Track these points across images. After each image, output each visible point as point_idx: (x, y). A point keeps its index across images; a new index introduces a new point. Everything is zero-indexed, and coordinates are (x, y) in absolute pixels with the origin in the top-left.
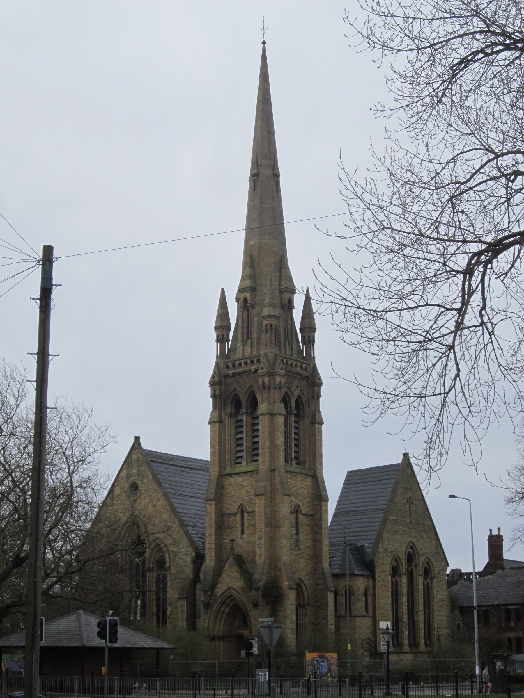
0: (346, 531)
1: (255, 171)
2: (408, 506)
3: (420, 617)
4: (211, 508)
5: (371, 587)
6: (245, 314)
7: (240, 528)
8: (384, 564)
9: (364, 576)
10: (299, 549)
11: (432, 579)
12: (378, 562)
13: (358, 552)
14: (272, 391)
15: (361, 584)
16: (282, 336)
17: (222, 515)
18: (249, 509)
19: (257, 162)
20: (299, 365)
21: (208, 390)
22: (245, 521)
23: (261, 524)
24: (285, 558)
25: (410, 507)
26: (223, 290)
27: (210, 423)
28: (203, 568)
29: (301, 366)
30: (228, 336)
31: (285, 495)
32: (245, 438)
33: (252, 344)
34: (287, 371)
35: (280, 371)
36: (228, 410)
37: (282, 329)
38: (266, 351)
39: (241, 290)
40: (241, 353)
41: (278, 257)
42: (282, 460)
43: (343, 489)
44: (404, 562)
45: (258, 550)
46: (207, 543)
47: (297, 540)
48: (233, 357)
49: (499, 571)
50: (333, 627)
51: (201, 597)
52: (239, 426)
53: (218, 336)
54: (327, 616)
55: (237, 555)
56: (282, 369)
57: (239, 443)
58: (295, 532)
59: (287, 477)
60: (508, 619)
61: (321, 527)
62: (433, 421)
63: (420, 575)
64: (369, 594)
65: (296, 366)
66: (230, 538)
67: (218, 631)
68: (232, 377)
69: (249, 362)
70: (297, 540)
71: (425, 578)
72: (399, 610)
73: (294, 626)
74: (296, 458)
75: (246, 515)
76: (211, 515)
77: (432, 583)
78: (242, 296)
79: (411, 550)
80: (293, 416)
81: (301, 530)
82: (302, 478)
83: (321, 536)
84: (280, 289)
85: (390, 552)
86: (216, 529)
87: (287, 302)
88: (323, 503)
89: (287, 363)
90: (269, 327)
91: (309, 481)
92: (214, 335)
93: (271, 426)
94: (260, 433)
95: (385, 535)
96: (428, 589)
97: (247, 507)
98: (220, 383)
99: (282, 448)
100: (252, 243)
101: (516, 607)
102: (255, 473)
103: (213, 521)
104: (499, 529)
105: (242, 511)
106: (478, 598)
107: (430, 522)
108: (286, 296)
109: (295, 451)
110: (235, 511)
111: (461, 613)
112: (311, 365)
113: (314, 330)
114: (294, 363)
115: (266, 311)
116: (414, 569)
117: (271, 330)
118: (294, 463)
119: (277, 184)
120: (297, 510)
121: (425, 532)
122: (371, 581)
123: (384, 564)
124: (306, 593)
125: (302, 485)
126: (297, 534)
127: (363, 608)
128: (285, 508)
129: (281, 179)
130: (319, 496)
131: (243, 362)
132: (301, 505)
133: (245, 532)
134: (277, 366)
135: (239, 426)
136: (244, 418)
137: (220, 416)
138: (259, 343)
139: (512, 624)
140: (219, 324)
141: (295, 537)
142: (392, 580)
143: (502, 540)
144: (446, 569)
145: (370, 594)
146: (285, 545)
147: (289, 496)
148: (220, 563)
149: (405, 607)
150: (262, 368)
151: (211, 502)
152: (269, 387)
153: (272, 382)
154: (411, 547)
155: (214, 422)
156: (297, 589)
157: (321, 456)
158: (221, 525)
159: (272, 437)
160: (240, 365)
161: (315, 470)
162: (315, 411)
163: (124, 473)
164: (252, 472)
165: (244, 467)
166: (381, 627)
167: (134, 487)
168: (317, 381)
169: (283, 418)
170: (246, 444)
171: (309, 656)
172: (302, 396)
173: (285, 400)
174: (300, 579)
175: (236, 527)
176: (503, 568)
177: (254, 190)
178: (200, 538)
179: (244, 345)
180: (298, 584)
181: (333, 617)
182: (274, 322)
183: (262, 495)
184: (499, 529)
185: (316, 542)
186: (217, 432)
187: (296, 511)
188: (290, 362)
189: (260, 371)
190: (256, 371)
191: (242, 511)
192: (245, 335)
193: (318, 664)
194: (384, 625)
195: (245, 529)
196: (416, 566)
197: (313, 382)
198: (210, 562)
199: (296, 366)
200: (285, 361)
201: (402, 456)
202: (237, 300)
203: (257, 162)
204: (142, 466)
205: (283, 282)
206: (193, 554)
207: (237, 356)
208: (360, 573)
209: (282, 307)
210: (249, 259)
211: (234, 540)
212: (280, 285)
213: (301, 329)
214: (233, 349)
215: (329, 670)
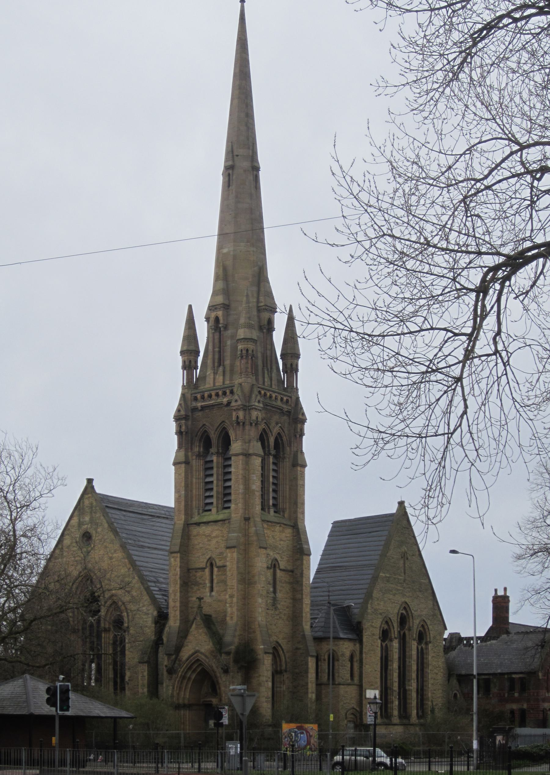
1: (230, 163)
2: (402, 562)
3: (413, 686)
4: (176, 562)
5: (358, 653)
6: (217, 336)
7: (208, 585)
9: (350, 640)
10: (276, 609)
11: (427, 644)
12: (366, 625)
14: (247, 427)
15: (346, 648)
16: (260, 363)
17: (189, 570)
18: (219, 563)
19: (232, 151)
20: (279, 398)
21: (173, 426)
22: (214, 577)
23: (233, 581)
24: (260, 619)
25: (404, 563)
26: (190, 307)
27: (175, 464)
28: (167, 629)
29: (282, 399)
30: (196, 362)
31: (260, 547)
32: (215, 482)
33: (224, 372)
34: (266, 405)
35: (257, 404)
36: (196, 449)
37: (259, 355)
38: (240, 381)
39: (212, 308)
41: (256, 269)
42: (258, 508)
43: (328, 541)
44: (395, 625)
45: (229, 610)
46: (171, 601)
47: (275, 599)
49: (504, 636)
51: (164, 661)
53: (184, 362)
54: (307, 683)
55: (205, 615)
56: (259, 402)
58: (271, 589)
59: (263, 527)
60: (512, 689)
61: (302, 585)
63: (414, 640)
64: (355, 659)
65: (276, 398)
67: (184, 698)
68: (201, 410)
69: (220, 393)
70: (275, 599)
72: (389, 678)
74: (274, 505)
75: (215, 569)
78: (213, 315)
79: (404, 612)
81: (278, 587)
83: (302, 594)
84: (258, 307)
85: (381, 614)
86: (182, 586)
87: (266, 323)
89: (265, 395)
90: (244, 352)
91: (289, 532)
92: (179, 360)
93: (246, 469)
94: (233, 477)
95: (376, 594)
97: (217, 561)
98: (186, 418)
99: (258, 494)
100: (225, 251)
103: (178, 577)
104: (505, 589)
105: (212, 565)
107: (427, 581)
108: (265, 315)
109: (274, 498)
110: (203, 565)
111: (459, 681)
112: (294, 398)
113: (298, 356)
114: (274, 395)
115: (242, 333)
116: (407, 632)
117: (247, 356)
118: (272, 511)
121: (420, 591)
122: (358, 645)
123: (372, 626)
125: (280, 537)
126: (275, 592)
127: (348, 676)
128: (260, 563)
130: (300, 550)
131: (213, 393)
132: (279, 559)
133: (215, 589)
135: (208, 468)
136: (215, 458)
137: (186, 456)
138: (232, 371)
139: (516, 695)
140: (185, 348)
141: (272, 595)
143: (509, 601)
144: (444, 633)
145: (357, 660)
146: (260, 605)
147: (266, 548)
150: (236, 401)
151: (175, 555)
152: (244, 423)
153: (247, 418)
154: (405, 608)
156: (273, 654)
157: (303, 504)
158: (188, 580)
159: (247, 481)
160: (210, 396)
161: (296, 519)
163: (75, 520)
165: (213, 515)
166: (368, 696)
167: (87, 537)
168: (300, 416)
169: (260, 459)
171: (286, 727)
172: (282, 434)
174: (277, 642)
175: (205, 583)
176: (508, 633)
177: (229, 186)
179: (215, 373)
180: (274, 648)
181: (314, 685)
182: (251, 346)
183: (234, 547)
184: (505, 589)
187: (274, 566)
188: (268, 394)
189: (233, 404)
190: (229, 404)
191: (212, 565)
192: (216, 361)
193: (296, 735)
194: (371, 693)
195: (215, 585)
196: (409, 630)
197: (295, 418)
198: (174, 622)
199: (276, 398)
200: (263, 392)
201: (397, 505)
202: (208, 319)
203: (232, 151)
204: (95, 513)
205: (262, 298)
207: (207, 386)
208: (345, 637)
209: (261, 328)
211: (203, 598)
213: (283, 356)
214: (202, 378)
215: (309, 743)
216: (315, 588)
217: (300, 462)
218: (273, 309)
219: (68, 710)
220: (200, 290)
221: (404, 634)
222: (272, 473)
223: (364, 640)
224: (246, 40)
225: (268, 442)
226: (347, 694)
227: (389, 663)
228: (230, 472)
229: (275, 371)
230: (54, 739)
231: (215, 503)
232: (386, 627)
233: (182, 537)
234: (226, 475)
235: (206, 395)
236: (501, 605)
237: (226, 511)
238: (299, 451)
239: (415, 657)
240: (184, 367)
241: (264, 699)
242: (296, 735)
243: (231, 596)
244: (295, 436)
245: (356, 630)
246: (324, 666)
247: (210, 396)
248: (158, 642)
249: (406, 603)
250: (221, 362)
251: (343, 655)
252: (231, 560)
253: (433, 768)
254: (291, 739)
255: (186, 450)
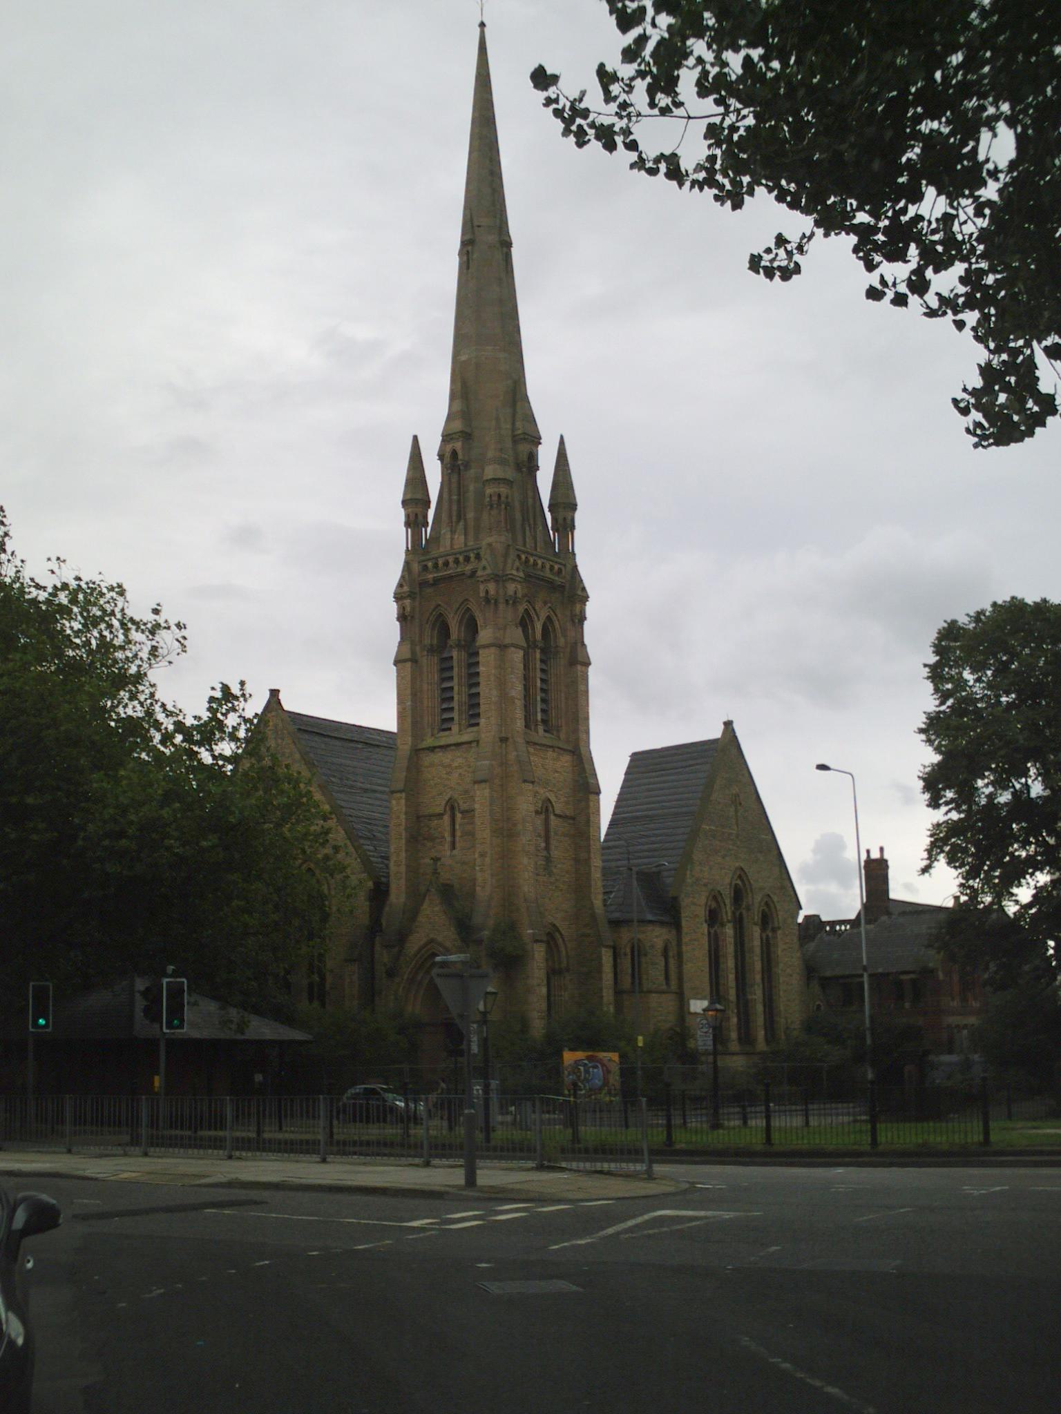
0: (631, 849)
1: (467, 237)
2: (732, 809)
3: (757, 994)
5: (674, 943)
6: (455, 479)
7: (449, 839)
8: (695, 904)
9: (662, 923)
10: (550, 874)
11: (774, 930)
12: (685, 902)
13: (651, 881)
14: (502, 606)
15: (657, 937)
16: (518, 516)
17: (418, 817)
18: (464, 807)
19: (472, 220)
20: (548, 566)
21: (393, 608)
22: (457, 827)
23: (483, 831)
24: (526, 889)
25: (736, 811)
26: (415, 438)
27: (396, 663)
28: (387, 909)
29: (552, 568)
30: (426, 517)
31: (525, 781)
32: (456, 688)
33: (466, 528)
34: (528, 576)
35: (514, 572)
36: (427, 641)
37: (517, 504)
38: (489, 540)
39: (447, 437)
40: (448, 543)
41: (510, 382)
42: (520, 724)
43: (625, 781)
44: (728, 901)
45: (479, 875)
46: (392, 864)
47: (548, 859)
48: (434, 553)
49: (884, 918)
50: (612, 1009)
51: (383, 957)
52: (445, 667)
53: (407, 516)
54: (601, 989)
55: (443, 885)
56: (518, 569)
57: (446, 696)
58: (543, 845)
59: (528, 752)
61: (588, 839)
62: (356, 1138)
63: (756, 924)
64: (671, 954)
65: (543, 566)
66: (434, 854)
68: (433, 585)
69: (461, 559)
70: (548, 859)
71: (764, 929)
72: (722, 982)
73: (544, 1006)
74: (544, 721)
75: (459, 815)
76: (398, 817)
77: (775, 938)
78: (449, 448)
79: (739, 882)
80: (538, 651)
81: (553, 843)
82: (555, 755)
83: (589, 852)
84: (514, 436)
85: (705, 885)
86: (408, 841)
87: (525, 458)
88: (592, 797)
89: (527, 560)
90: (495, 498)
92: (401, 514)
93: (501, 671)
94: (482, 679)
95: (698, 856)
96: (767, 947)
97: (461, 802)
98: (412, 595)
99: (519, 703)
100: (463, 358)
101: (912, 976)
102: (474, 744)
103: (403, 827)
104: (882, 849)
105: (452, 808)
106: (868, 958)
107: (769, 837)
108: (524, 448)
109: (543, 711)
110: (439, 810)
111: (823, 987)
112: (569, 567)
113: (573, 507)
114: (540, 562)
115: (490, 472)
116: (744, 912)
117: (499, 504)
118: (541, 728)
119: (508, 258)
120: (547, 810)
122: (674, 932)
123: (695, 904)
124: (563, 949)
125: (557, 766)
127: (662, 978)
128: (525, 805)
129: (513, 250)
130: (587, 787)
131: (451, 559)
132: (553, 799)
133: (458, 845)
134: (509, 566)
135: (445, 667)
136: (455, 654)
137: (413, 652)
138: (478, 528)
139: (907, 1005)
140: (408, 497)
141: (545, 853)
142: (709, 933)
143: (887, 867)
144: (798, 914)
145: (674, 954)
146: (526, 867)
147: (533, 783)
148: (416, 897)
149: (732, 977)
150: (484, 568)
151: (398, 795)
152: (496, 602)
153: (501, 592)
154: (740, 877)
155: (405, 661)
156: (548, 943)
157: (587, 718)
158: (418, 834)
159: (502, 684)
160: (446, 564)
161: (577, 740)
162: (576, 643)
164: (470, 743)
165: (454, 736)
166: (692, 1009)
168: (579, 593)
169: (521, 653)
170: (459, 695)
171: (569, 1057)
172: (554, 618)
173: (525, 623)
174: (554, 925)
175: (443, 837)
176: (889, 914)
177: (468, 268)
178: (382, 857)
179: (453, 532)
180: (549, 934)
181: (611, 992)
182: (503, 490)
183: (485, 781)
184: (882, 849)
185: (581, 863)
186: (409, 678)
187: (545, 809)
189: (479, 573)
190: (474, 573)
191: (452, 808)
192: (454, 513)
193: (587, 1072)
194: (698, 1006)
195: (457, 839)
196: (748, 909)
197: (569, 593)
198: (398, 896)
199: (543, 566)
200: (523, 557)
201: (722, 727)
202: (441, 457)
203: (472, 220)
204: (283, 739)
205: (519, 424)
206: (370, 884)
207: (442, 550)
209: (518, 467)
210: (459, 384)
211: (439, 859)
212: (513, 429)
213: (552, 507)
214: (435, 539)
215: (606, 1082)
216: (609, 848)
217: (580, 659)
218: (536, 440)
219: (181, 1026)
220: (425, 408)
221: (741, 914)
222: (539, 674)
223: (684, 923)
224: (488, 75)
225: (533, 629)
226: (661, 1009)
227: (722, 960)
228: (478, 674)
229: (539, 523)
230: (157, 1078)
231: (456, 718)
232: (714, 905)
233: (408, 769)
234: (473, 678)
235: (440, 562)
236: (876, 872)
237: (475, 729)
238: (579, 644)
239: (758, 950)
240: (408, 524)
241: (535, 1014)
242: (587, 1072)
243: (483, 855)
244: (573, 621)
245: (670, 912)
246: (626, 963)
247: (446, 564)
248: (375, 927)
249: (742, 869)
250: (461, 516)
251: (652, 946)
252: (482, 798)
253: (813, 1122)
254: (579, 1077)
255: (413, 643)
